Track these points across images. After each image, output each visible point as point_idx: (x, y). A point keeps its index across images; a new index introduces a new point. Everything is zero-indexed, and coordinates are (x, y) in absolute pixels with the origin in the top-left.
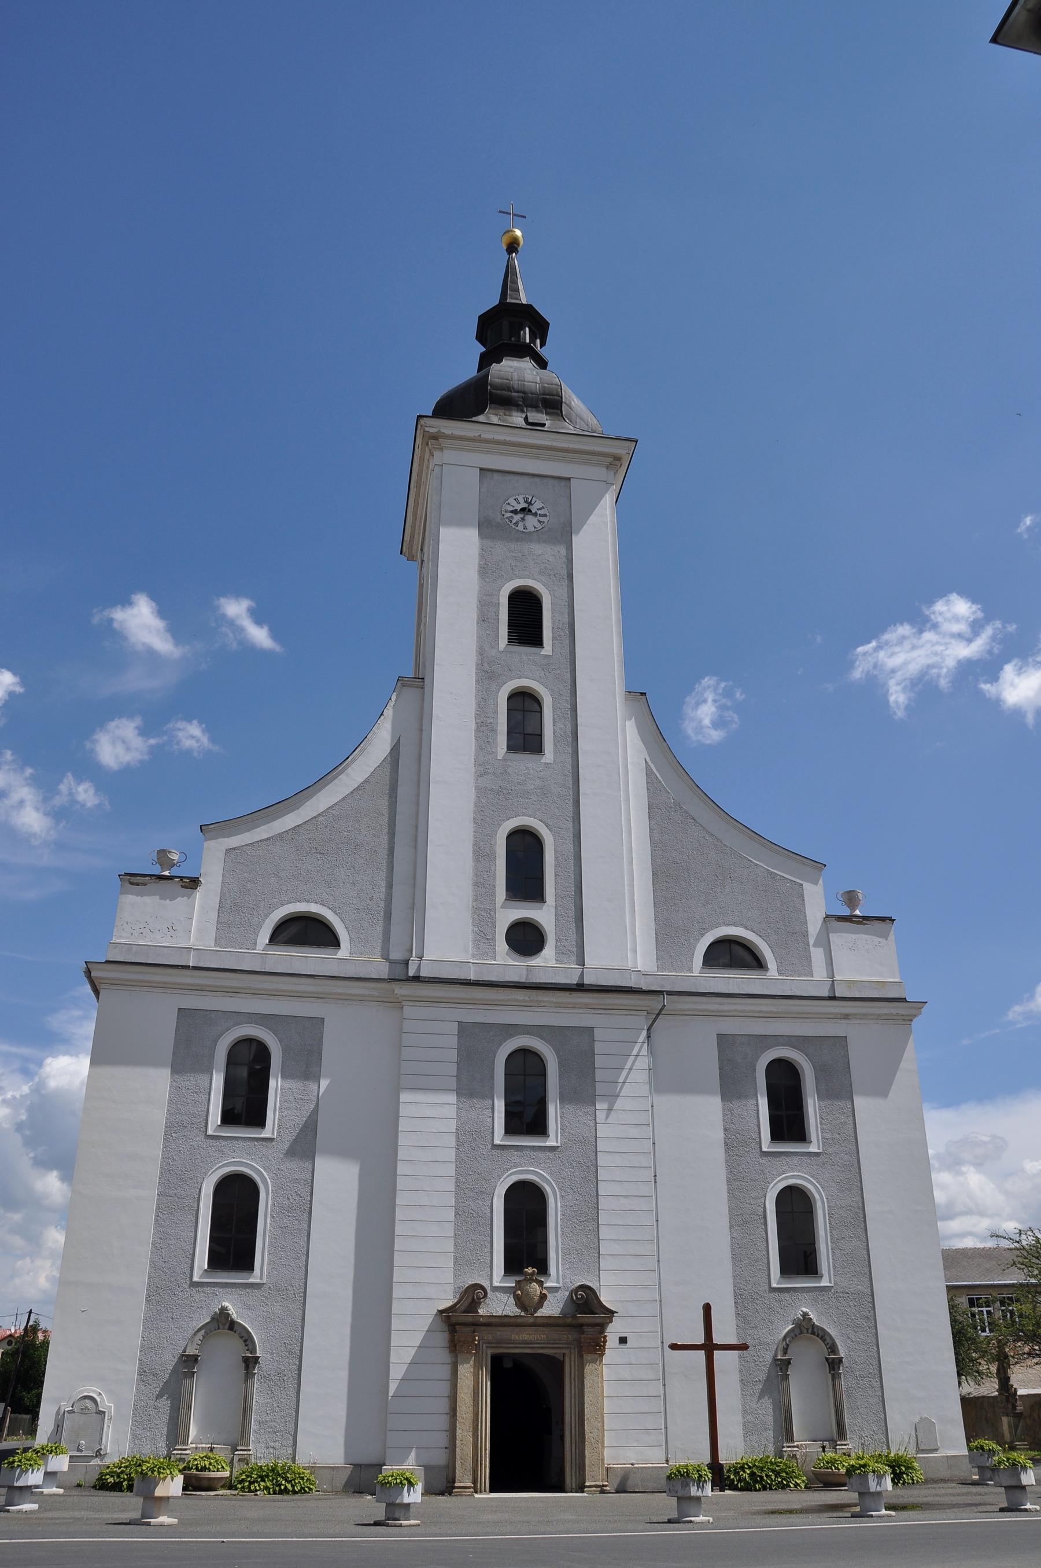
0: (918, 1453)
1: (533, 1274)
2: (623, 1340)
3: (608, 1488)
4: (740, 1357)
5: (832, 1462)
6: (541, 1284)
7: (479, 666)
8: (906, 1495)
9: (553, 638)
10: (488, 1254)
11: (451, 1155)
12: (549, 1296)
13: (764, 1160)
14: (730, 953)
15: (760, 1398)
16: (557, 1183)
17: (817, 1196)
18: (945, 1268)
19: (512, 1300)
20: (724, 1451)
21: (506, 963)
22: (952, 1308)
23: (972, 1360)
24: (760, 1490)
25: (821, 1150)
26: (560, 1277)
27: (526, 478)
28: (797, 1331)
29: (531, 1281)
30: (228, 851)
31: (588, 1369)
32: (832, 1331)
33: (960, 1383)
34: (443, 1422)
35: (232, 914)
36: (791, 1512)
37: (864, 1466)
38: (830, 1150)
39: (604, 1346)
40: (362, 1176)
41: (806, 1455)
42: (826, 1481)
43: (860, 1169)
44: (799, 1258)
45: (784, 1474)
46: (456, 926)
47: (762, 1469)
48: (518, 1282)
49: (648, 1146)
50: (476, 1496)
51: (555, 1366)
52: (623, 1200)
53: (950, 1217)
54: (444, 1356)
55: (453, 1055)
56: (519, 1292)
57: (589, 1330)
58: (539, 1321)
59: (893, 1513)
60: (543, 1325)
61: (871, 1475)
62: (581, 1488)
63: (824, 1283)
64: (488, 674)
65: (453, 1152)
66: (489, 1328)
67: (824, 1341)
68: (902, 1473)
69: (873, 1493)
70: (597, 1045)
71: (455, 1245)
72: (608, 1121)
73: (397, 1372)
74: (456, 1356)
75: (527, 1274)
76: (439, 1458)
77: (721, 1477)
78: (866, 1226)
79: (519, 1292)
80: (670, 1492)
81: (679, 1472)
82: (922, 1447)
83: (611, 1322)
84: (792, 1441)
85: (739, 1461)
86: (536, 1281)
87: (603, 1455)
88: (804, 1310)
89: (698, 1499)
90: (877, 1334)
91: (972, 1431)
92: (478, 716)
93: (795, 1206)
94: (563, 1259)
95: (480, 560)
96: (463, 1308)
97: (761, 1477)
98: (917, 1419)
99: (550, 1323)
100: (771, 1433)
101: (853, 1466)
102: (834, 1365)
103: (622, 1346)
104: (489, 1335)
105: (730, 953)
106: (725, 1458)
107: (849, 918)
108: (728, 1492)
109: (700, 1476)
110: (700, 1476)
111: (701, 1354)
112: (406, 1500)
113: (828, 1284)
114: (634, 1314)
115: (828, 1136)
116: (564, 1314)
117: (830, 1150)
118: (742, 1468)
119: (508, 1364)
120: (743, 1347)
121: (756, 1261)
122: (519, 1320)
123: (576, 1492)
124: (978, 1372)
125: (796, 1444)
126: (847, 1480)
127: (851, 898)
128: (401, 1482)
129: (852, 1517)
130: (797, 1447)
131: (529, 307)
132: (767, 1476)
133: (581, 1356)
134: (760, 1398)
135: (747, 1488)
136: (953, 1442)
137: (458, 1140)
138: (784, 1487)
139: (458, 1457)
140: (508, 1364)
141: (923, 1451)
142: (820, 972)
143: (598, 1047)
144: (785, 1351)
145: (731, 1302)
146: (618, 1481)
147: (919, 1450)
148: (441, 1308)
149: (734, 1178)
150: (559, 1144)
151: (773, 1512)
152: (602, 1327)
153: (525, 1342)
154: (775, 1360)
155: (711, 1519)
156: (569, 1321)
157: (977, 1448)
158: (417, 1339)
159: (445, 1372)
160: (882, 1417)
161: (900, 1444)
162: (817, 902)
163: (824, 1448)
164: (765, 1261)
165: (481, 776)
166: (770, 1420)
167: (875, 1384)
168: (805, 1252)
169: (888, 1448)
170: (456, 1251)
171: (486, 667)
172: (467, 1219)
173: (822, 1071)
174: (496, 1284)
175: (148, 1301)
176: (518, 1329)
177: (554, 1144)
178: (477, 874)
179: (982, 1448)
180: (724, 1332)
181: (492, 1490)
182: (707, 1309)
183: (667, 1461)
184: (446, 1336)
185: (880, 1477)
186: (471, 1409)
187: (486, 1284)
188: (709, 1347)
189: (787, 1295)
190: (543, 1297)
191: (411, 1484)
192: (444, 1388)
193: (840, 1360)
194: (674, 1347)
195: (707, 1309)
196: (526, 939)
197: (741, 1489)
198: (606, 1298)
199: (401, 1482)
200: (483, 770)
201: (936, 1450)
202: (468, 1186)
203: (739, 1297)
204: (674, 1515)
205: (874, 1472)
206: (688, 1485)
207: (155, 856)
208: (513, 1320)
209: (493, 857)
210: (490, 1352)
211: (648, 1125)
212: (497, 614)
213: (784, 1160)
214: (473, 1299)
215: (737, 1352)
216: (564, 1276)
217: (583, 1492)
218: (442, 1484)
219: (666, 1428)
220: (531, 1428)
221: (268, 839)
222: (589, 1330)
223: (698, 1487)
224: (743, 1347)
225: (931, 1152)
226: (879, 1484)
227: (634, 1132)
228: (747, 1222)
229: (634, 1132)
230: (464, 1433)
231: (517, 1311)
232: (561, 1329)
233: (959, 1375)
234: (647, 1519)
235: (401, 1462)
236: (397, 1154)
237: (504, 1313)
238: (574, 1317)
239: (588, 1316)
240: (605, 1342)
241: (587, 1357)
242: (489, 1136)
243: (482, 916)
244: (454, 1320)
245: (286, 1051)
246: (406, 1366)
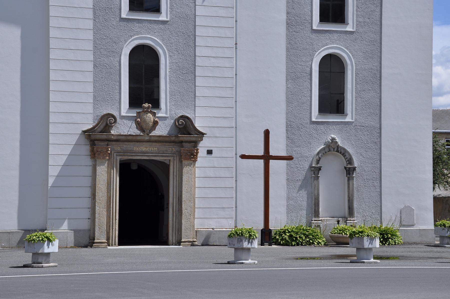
0: (400, 226)
1: (148, 107)
2: (210, 152)
3: (196, 243)
4: (287, 165)
5: (343, 230)
6: (154, 114)
8: (388, 250)
10: (118, 94)
11: (90, 24)
12: (160, 123)
13: (314, 36)
15: (299, 190)
16: (167, 46)
17: (348, 62)
18: (434, 121)
19: (134, 125)
20: (274, 222)
22: (435, 142)
23: (444, 175)
24: (295, 245)
25: (354, 30)
26: (167, 111)
28: (327, 150)
29: (147, 112)
31: (185, 170)
32: (350, 150)
33: (434, 188)
34: (87, 202)
36: (314, 258)
37: (362, 232)
38: (361, 30)
39: (197, 155)
40: (23, 37)
41: (326, 226)
42: (338, 242)
43: (381, 43)
44: (332, 103)
45: (311, 237)
47: (297, 233)
48: (138, 113)
49: (232, 23)
50: (109, 247)
52: (213, 60)
53: (440, 94)
54: (88, 161)
56: (139, 120)
57: (186, 145)
58: (153, 139)
59: (378, 261)
60: (156, 142)
61: (365, 238)
62: (179, 243)
63: (348, 119)
66: (118, 143)
67: (344, 156)
68: (388, 238)
69: (366, 249)
71: (94, 87)
72: (205, 4)
73: (53, 172)
74: (96, 161)
75: (144, 108)
76: (85, 225)
77: (267, 237)
78: (381, 83)
79: (139, 120)
80: (230, 245)
81: (237, 233)
82: (403, 223)
83: (202, 140)
84: (318, 217)
85: (283, 228)
86: (151, 112)
87: (194, 223)
88: (333, 136)
89: (249, 249)
90: (381, 153)
91: (438, 215)
93: (332, 68)
94: (170, 99)
96: (100, 130)
97: (296, 238)
98: (402, 206)
99: (160, 140)
100: (305, 212)
101: (354, 232)
102: (350, 171)
103: (209, 156)
104: (118, 147)
106: (272, 226)
108: (274, 246)
109: (250, 235)
110: (250, 235)
111: (261, 162)
112: (46, 250)
113: (351, 120)
114: (218, 135)
115: (361, 20)
116: (169, 135)
117: (361, 30)
118: (284, 232)
119: (134, 167)
120: (289, 158)
121: (303, 103)
122: (139, 138)
123: (175, 245)
124: (447, 182)
125: (320, 219)
126: (349, 240)
128: (42, 240)
129: (351, 262)
130: (321, 220)
132: (300, 237)
133: (181, 162)
134: (299, 190)
135: (287, 244)
136: (426, 221)
137: (95, 13)
138: (310, 244)
139: (97, 224)
140: (134, 167)
141: (404, 226)
144: (318, 162)
145: (283, 129)
146: (203, 239)
147: (401, 225)
148: (85, 129)
149: (293, 49)
150: (168, 19)
151: (302, 259)
152: (195, 143)
153: (144, 152)
154: (311, 167)
155: (256, 262)
156: (173, 139)
157: (441, 225)
158: (68, 150)
159: (88, 171)
160: (379, 204)
161: (389, 221)
163: (338, 222)
164: (309, 103)
166: (305, 204)
167: (376, 184)
168: (338, 101)
169: (381, 223)
170: (95, 91)
172: (103, 71)
174: (123, 114)
176: (138, 144)
177: (165, 19)
179: (444, 225)
181: (119, 245)
182: (267, 133)
184: (88, 148)
185: (372, 239)
186: (106, 194)
187: (116, 114)
188: (267, 157)
189: (322, 126)
190: (155, 123)
191: (49, 240)
192: (88, 182)
193: (354, 169)
194: (243, 157)
195: (267, 133)
197: (283, 245)
198: (199, 125)
199: (42, 240)
201: (413, 225)
202: (103, 48)
203: (289, 127)
204: (232, 259)
205: (368, 236)
206: (241, 241)
208: (134, 138)
210: (119, 158)
211: (233, 8)
213: (327, 35)
214: (107, 124)
215: (285, 161)
216: (171, 110)
217: (180, 245)
218: (86, 241)
219: (236, 207)
220: (146, 207)
222: (186, 145)
223: (249, 242)
224: (289, 158)
225: (434, 53)
226: (371, 243)
227: (222, 12)
228: (298, 78)
229: (222, 12)
230: (101, 210)
231: (138, 132)
232: (167, 144)
233: (434, 183)
234: (215, 261)
235: (58, 227)
236: (49, 22)
237: (129, 133)
238: (176, 136)
239: (186, 135)
240: (197, 153)
241: (185, 162)
242: (118, 12)
244: (93, 137)
246: (60, 168)
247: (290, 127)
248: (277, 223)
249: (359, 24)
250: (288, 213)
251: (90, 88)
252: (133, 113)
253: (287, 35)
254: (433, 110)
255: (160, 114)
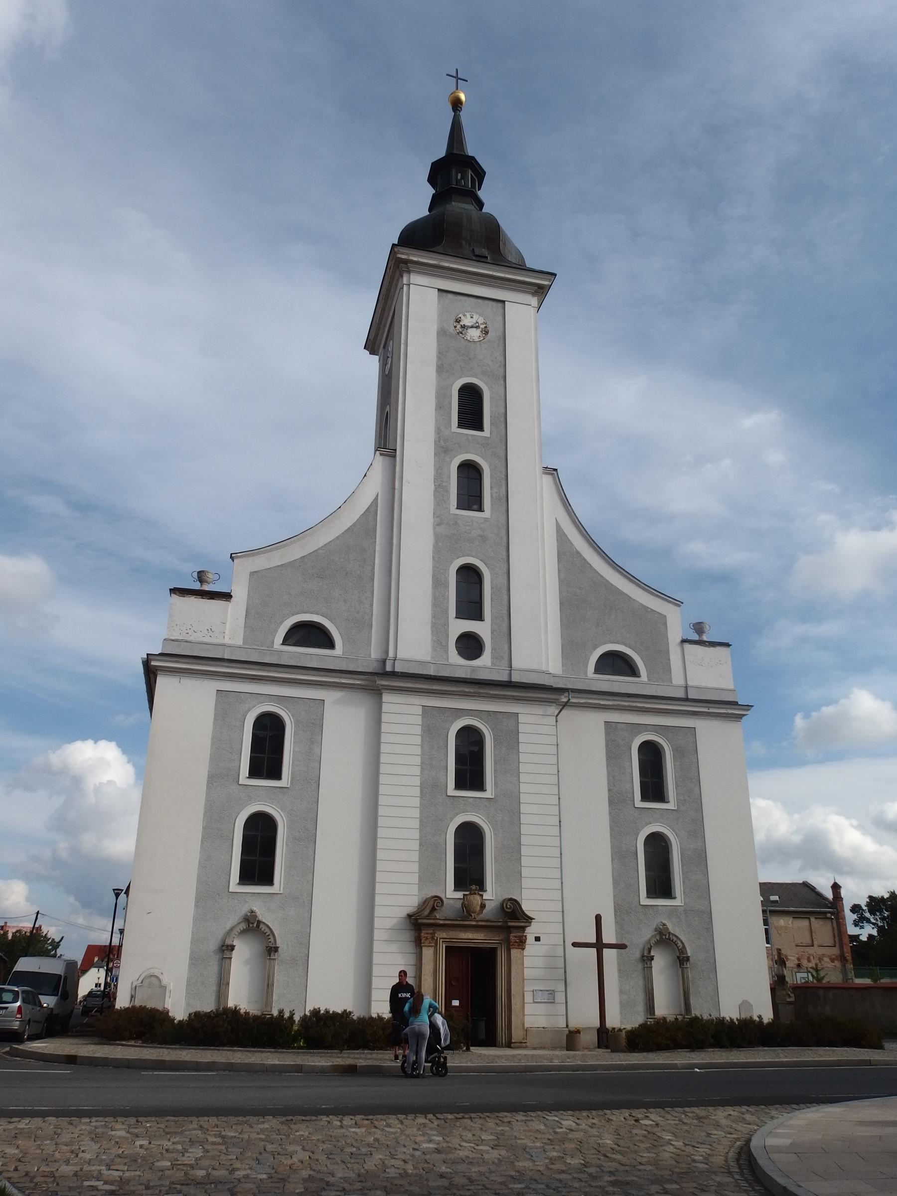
6: (482, 896)
7: (437, 443)
9: (491, 424)
14: (616, 663)
21: (456, 663)
26: (493, 894)
27: (472, 299)
30: (252, 574)
31: (514, 952)
35: (257, 616)
44: (660, 885)
46: (418, 635)
51: (493, 952)
54: (410, 947)
55: (418, 730)
64: (443, 449)
65: (417, 865)
70: (523, 849)
92: (435, 480)
93: (658, 846)
95: (437, 361)
104: (441, 935)
105: (616, 663)
107: (698, 637)
127: (699, 628)
131: (473, 158)
137: (421, 791)
142: (677, 679)
143: (522, 728)
162: (676, 627)
165: (438, 525)
171: (442, 443)
173: (679, 752)
175: (196, 906)
178: (435, 598)
180: (609, 937)
183: (567, 1026)
187: (442, 896)
188: (599, 946)
194: (575, 945)
196: (470, 645)
198: (526, 907)
200: (439, 520)
202: (429, 822)
207: (195, 575)
209: (447, 587)
212: (450, 404)
221: (282, 565)
239: (513, 919)
243: (439, 629)
245: (297, 723)
247: (619, 910)
248: (613, 1020)
249: (679, 802)
250: (621, 1010)
251: (415, 868)
252: (459, 895)
253: (610, 813)
254: (766, 889)
255: (486, 896)
